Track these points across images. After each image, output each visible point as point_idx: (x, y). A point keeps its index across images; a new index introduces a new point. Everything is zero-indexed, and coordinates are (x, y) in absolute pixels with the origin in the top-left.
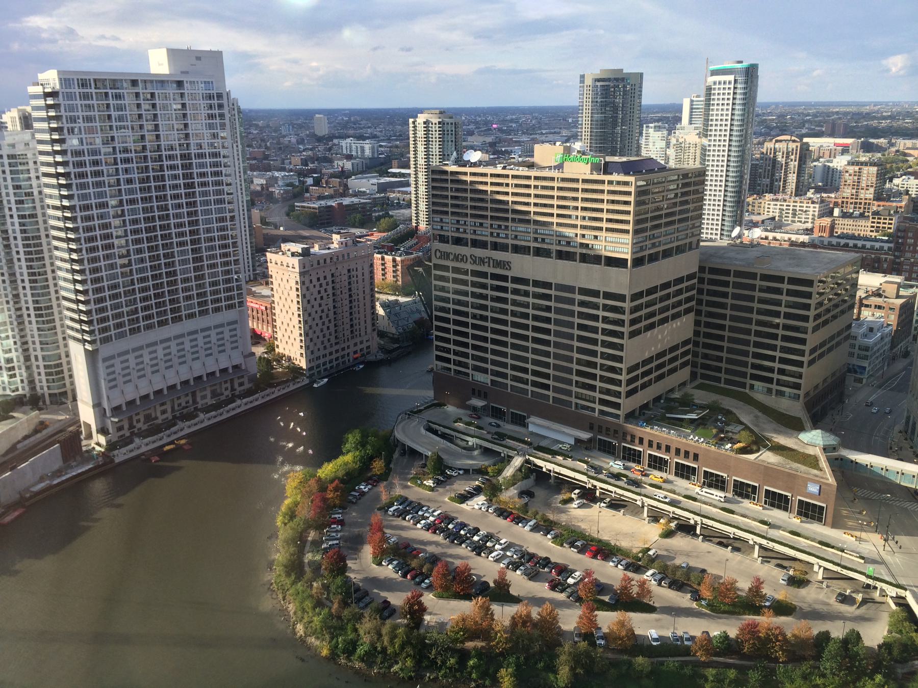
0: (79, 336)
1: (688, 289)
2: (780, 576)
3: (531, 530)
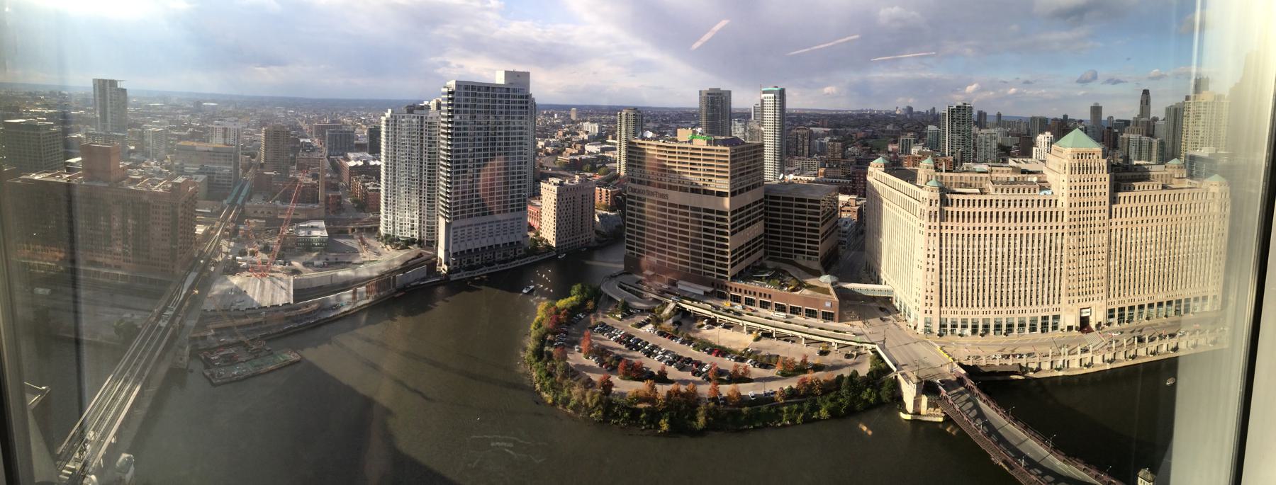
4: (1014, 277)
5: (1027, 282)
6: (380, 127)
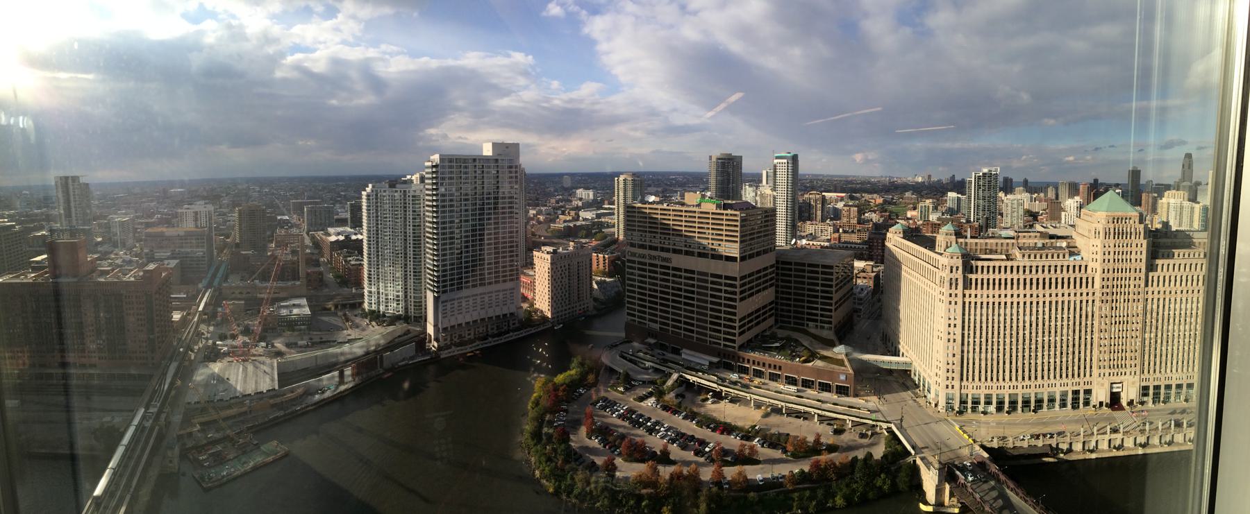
0: (432, 288)
2: (829, 430)
3: (683, 419)
4: (1043, 347)
5: (1057, 353)
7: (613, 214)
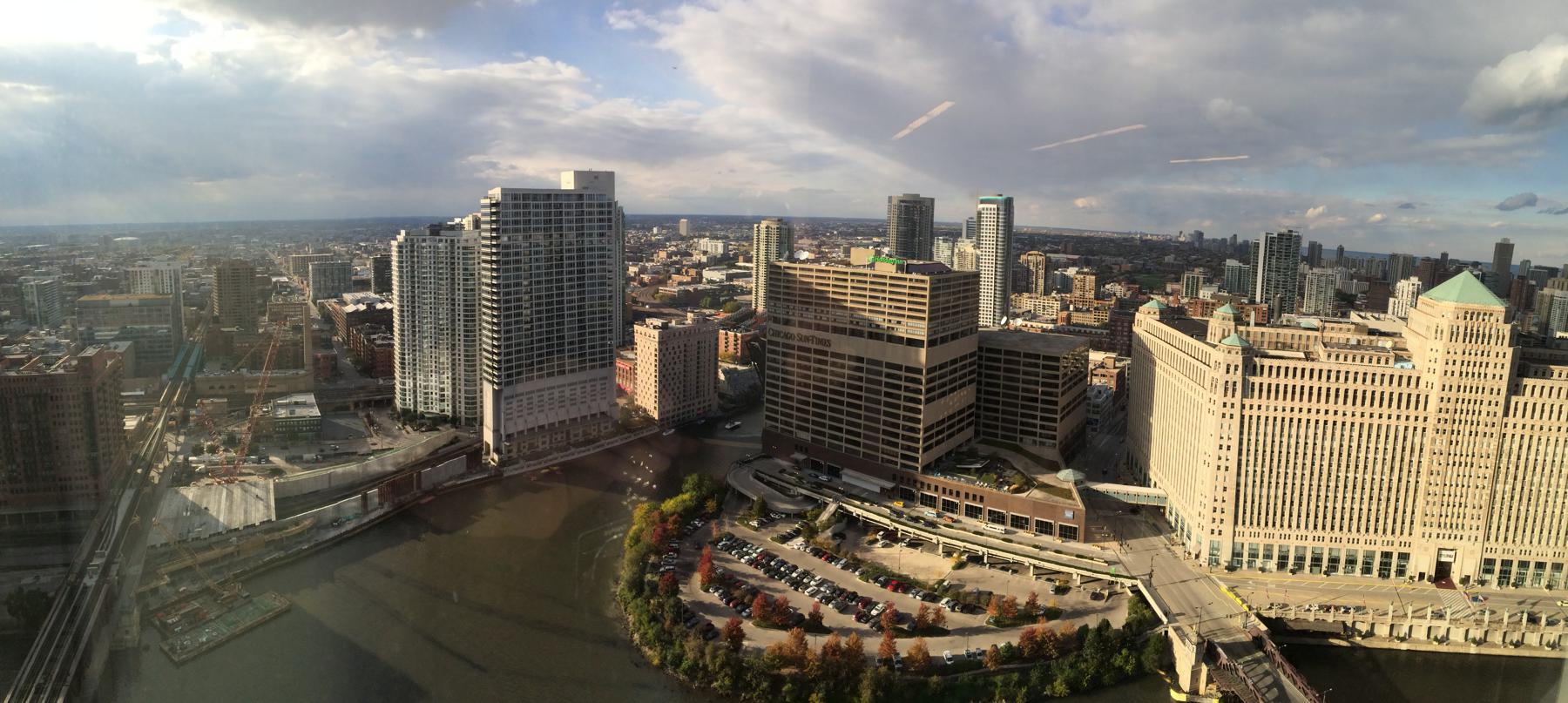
1: (971, 364)
4: (1346, 487)
6: (390, 256)
7: (750, 276)
